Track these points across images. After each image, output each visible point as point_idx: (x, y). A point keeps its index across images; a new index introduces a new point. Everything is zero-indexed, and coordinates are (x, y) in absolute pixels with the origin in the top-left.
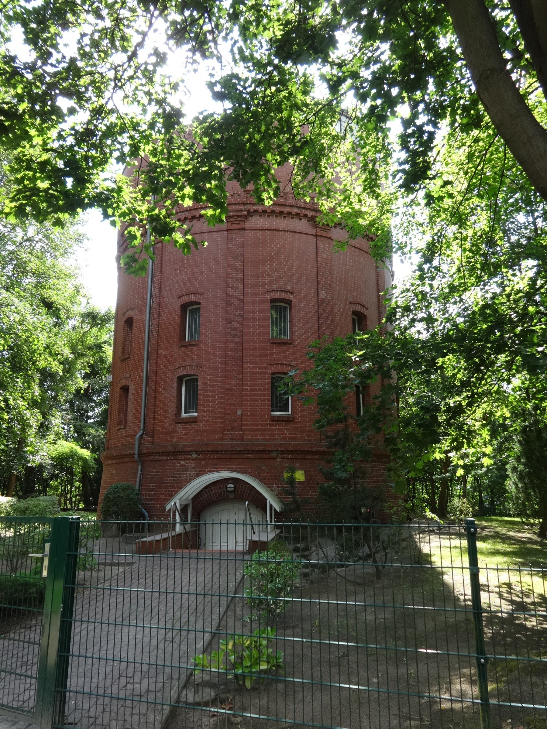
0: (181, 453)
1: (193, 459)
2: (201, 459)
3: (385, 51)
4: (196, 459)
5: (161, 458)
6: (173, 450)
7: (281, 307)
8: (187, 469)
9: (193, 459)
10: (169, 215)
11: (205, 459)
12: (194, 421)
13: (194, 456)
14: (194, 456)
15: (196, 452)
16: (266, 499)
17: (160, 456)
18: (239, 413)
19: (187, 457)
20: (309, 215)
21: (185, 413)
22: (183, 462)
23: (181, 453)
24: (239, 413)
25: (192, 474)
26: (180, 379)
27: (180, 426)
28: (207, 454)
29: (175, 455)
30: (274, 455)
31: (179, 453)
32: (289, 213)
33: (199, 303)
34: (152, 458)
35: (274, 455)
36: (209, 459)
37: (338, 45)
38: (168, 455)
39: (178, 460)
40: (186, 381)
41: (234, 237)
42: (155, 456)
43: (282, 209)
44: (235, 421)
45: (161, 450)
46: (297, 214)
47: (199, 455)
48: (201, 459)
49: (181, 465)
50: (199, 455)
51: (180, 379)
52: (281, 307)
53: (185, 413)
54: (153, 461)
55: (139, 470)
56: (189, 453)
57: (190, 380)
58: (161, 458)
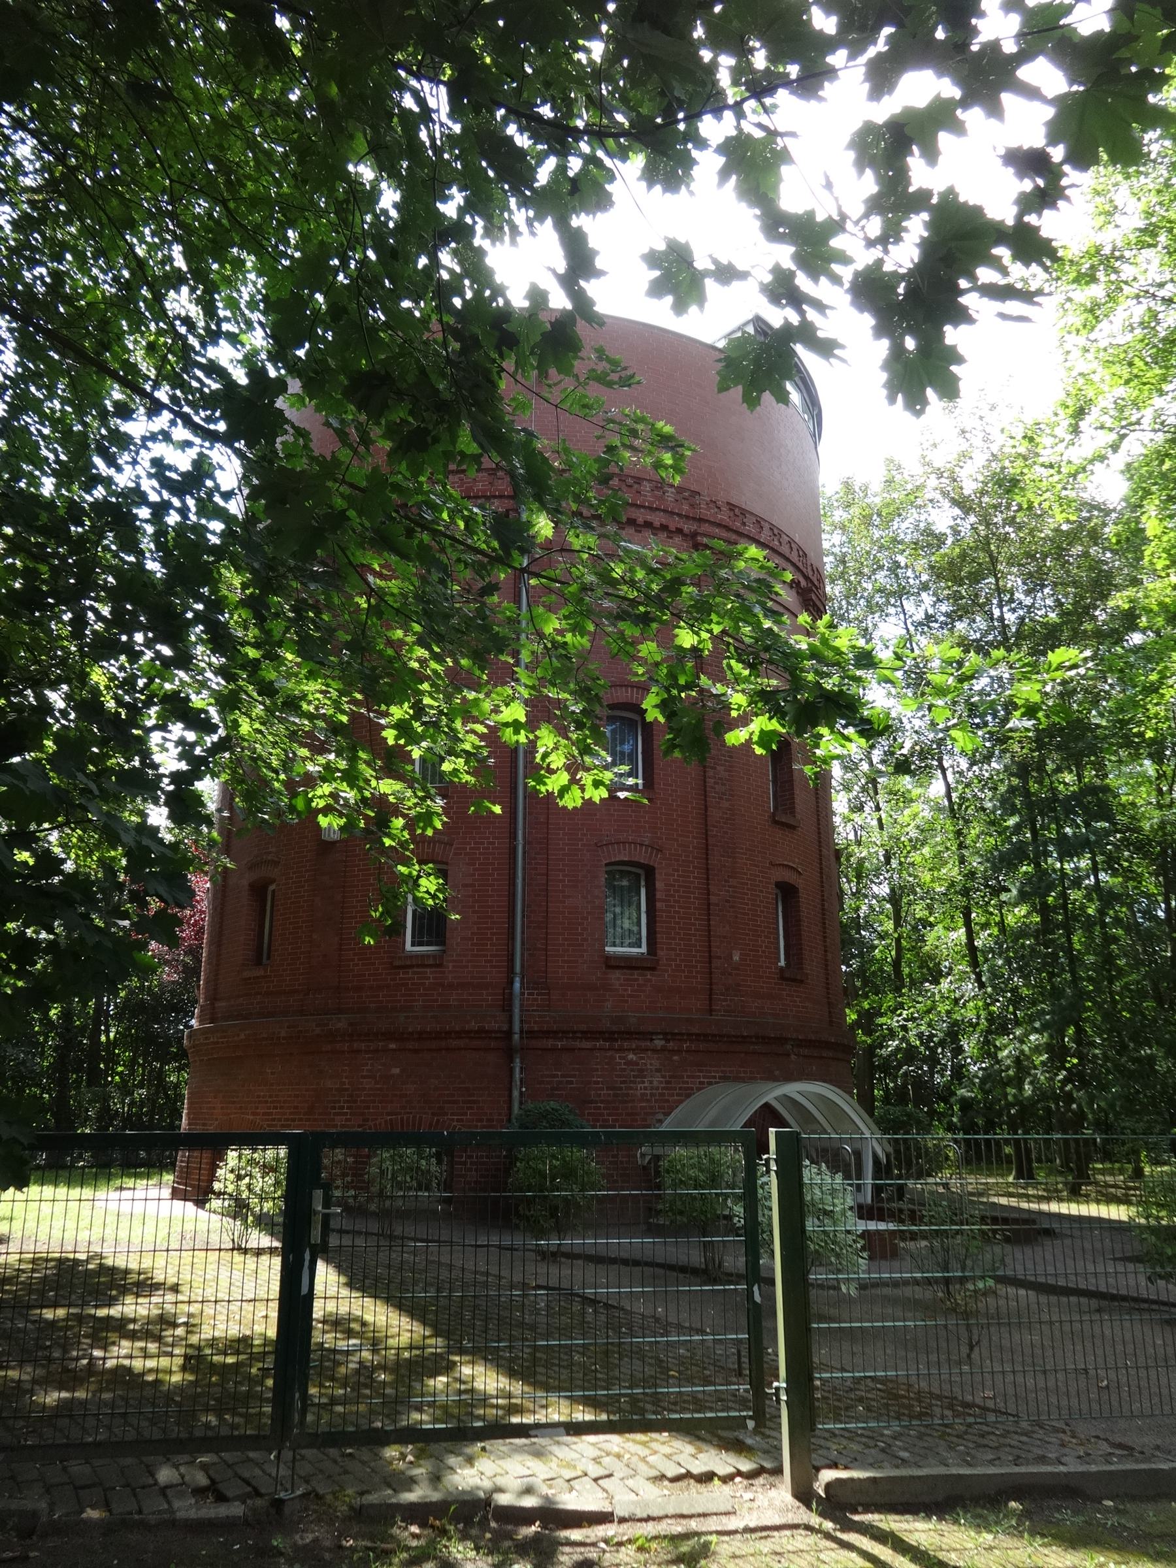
0: (629, 1035)
1: (655, 1051)
2: (673, 1052)
3: (743, 275)
4: (664, 1049)
5: (578, 1044)
6: (614, 1028)
8: (641, 1071)
9: (655, 1051)
10: (1063, 970)
11: (679, 1052)
13: (659, 1043)
14: (659, 1043)
15: (665, 1034)
18: (736, 958)
19: (643, 1044)
20: (686, 530)
22: (631, 1056)
23: (629, 1035)
24: (736, 958)
25: (655, 1084)
27: (617, 974)
29: (616, 1040)
31: (619, 1035)
32: (648, 525)
34: (550, 1043)
35: (789, 1047)
38: (597, 1039)
39: (621, 1050)
45: (584, 1027)
46: (664, 527)
47: (668, 1041)
48: (673, 1052)
50: (668, 1041)
54: (554, 1049)
55: (518, 1070)
56: (648, 1036)
58: (578, 1044)
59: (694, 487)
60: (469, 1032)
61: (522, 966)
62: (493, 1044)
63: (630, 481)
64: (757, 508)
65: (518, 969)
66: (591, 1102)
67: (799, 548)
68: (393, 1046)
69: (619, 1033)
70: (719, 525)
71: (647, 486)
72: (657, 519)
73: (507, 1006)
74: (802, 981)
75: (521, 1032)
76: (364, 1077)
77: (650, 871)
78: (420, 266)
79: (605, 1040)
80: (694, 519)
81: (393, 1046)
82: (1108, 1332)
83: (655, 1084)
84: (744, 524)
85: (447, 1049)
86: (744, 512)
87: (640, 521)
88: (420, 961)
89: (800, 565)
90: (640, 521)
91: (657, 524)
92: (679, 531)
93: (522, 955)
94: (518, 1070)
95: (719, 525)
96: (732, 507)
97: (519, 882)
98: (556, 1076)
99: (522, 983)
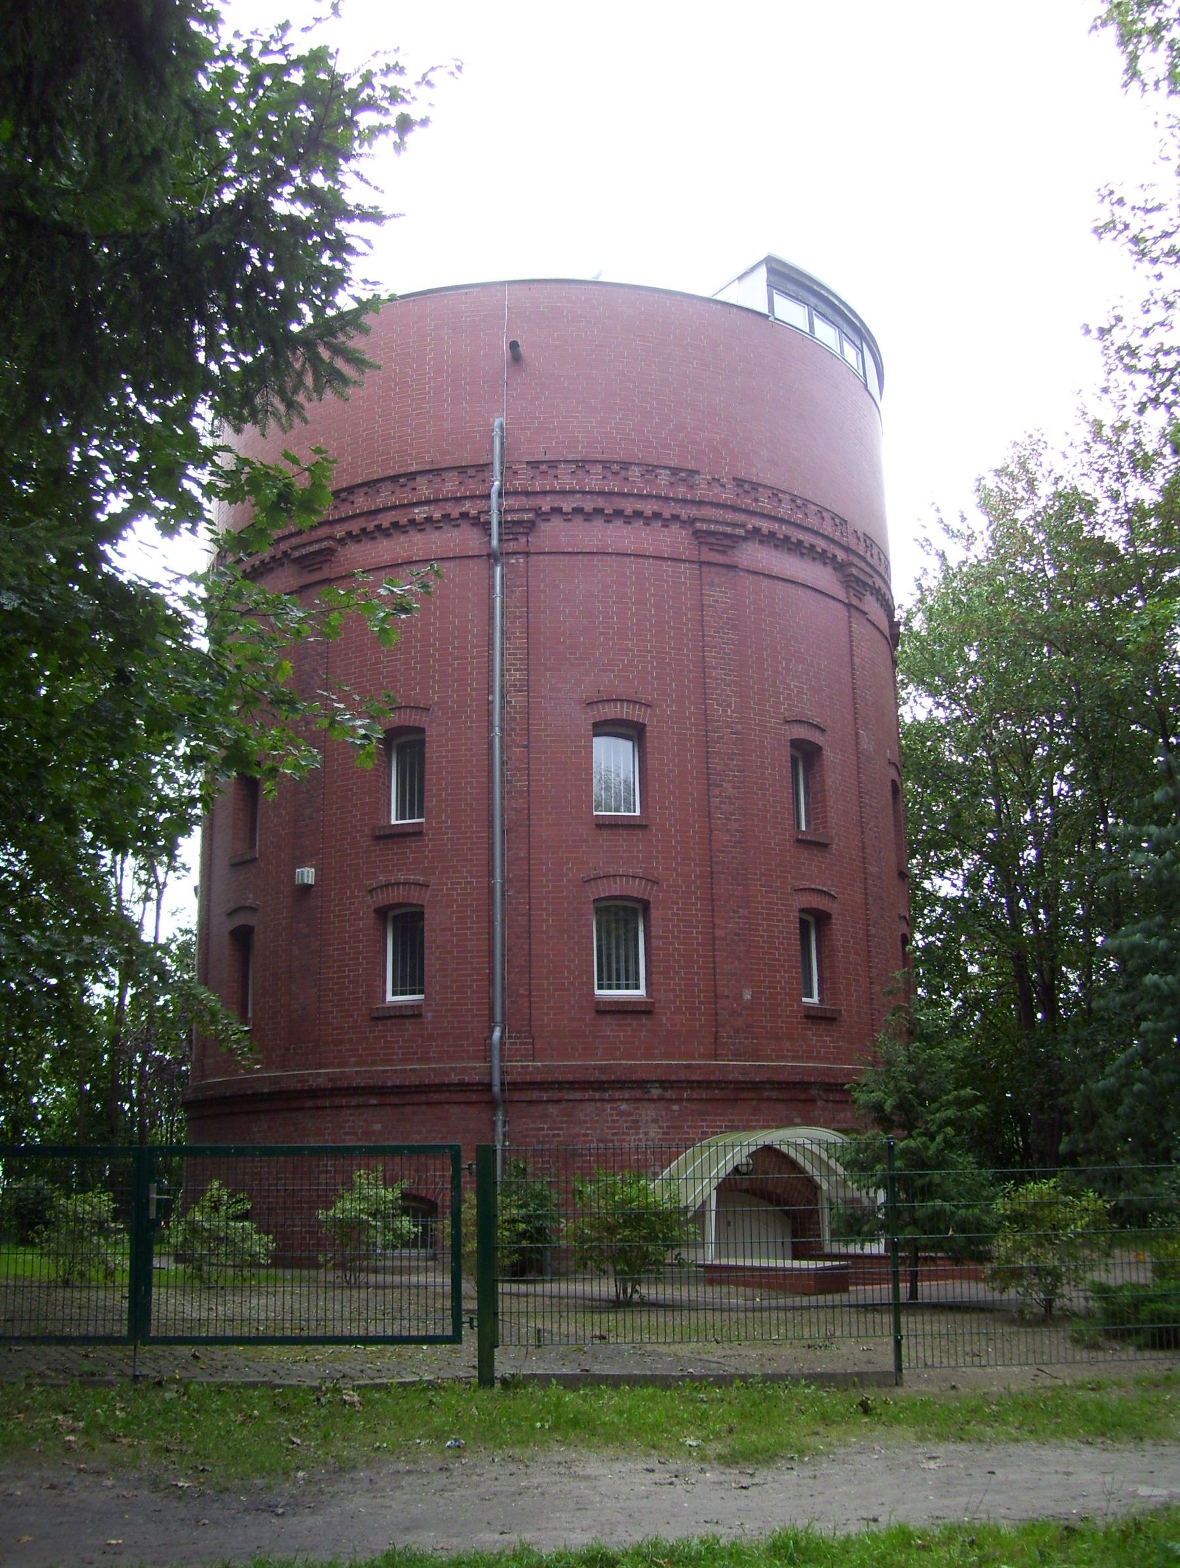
7: (806, 755)
11: (678, 1100)
12: (411, 1014)
13: (656, 1092)
16: (816, 1188)
17: (560, 1089)
18: (747, 996)
21: (394, 994)
22: (624, 1107)
24: (747, 996)
26: (382, 913)
28: (685, 1089)
30: (814, 1092)
32: (638, 514)
33: (422, 730)
34: (535, 1095)
35: (814, 1092)
36: (689, 1100)
37: (222, 16)
40: (396, 918)
41: (716, 580)
42: (546, 1090)
43: (639, 506)
44: (740, 1015)
49: (621, 1114)
51: (382, 913)
52: (806, 755)
53: (394, 994)
55: (500, 1123)
57: (405, 915)
59: (691, 466)
60: (449, 1085)
61: (503, 1015)
62: (474, 1097)
63: (616, 467)
64: (768, 478)
65: (498, 1017)
66: (582, 1155)
67: (835, 516)
68: (374, 1101)
69: (609, 1082)
70: (724, 506)
71: (636, 471)
72: (648, 508)
73: (486, 1055)
74: (833, 1019)
75: (502, 1084)
76: (346, 1134)
77: (646, 905)
78: (85, 569)
79: (594, 1090)
80: (693, 502)
81: (374, 1101)
82: (921, 1354)
83: (652, 1135)
84: (756, 500)
85: (428, 1104)
86: (755, 486)
87: (629, 511)
88: (400, 1014)
89: (837, 536)
90: (629, 511)
91: (648, 513)
92: (675, 517)
93: (503, 1003)
94: (500, 1123)
95: (724, 506)
96: (739, 482)
97: (498, 924)
98: (542, 1129)
99: (503, 1032)
